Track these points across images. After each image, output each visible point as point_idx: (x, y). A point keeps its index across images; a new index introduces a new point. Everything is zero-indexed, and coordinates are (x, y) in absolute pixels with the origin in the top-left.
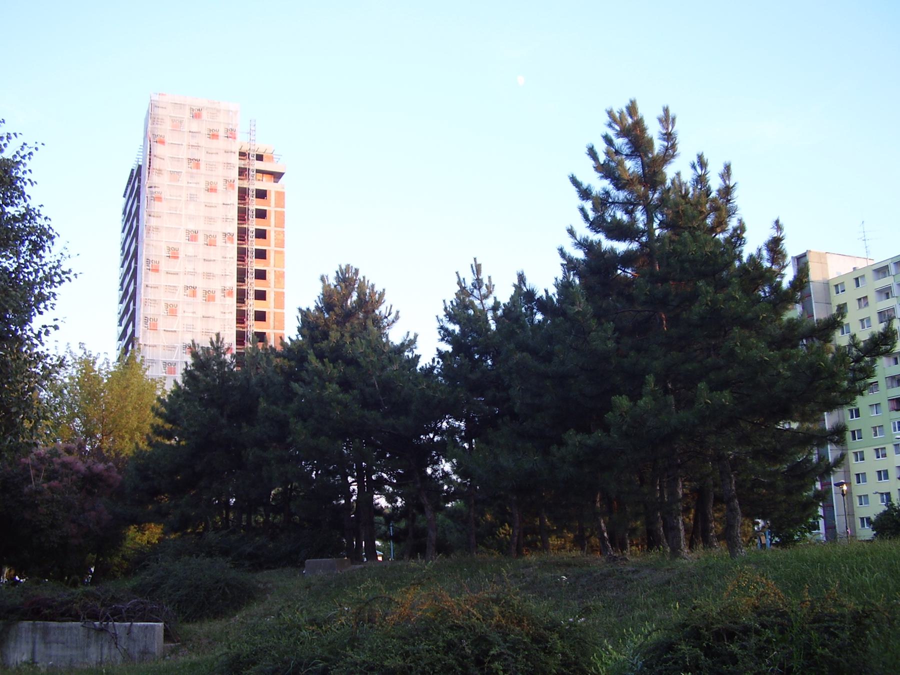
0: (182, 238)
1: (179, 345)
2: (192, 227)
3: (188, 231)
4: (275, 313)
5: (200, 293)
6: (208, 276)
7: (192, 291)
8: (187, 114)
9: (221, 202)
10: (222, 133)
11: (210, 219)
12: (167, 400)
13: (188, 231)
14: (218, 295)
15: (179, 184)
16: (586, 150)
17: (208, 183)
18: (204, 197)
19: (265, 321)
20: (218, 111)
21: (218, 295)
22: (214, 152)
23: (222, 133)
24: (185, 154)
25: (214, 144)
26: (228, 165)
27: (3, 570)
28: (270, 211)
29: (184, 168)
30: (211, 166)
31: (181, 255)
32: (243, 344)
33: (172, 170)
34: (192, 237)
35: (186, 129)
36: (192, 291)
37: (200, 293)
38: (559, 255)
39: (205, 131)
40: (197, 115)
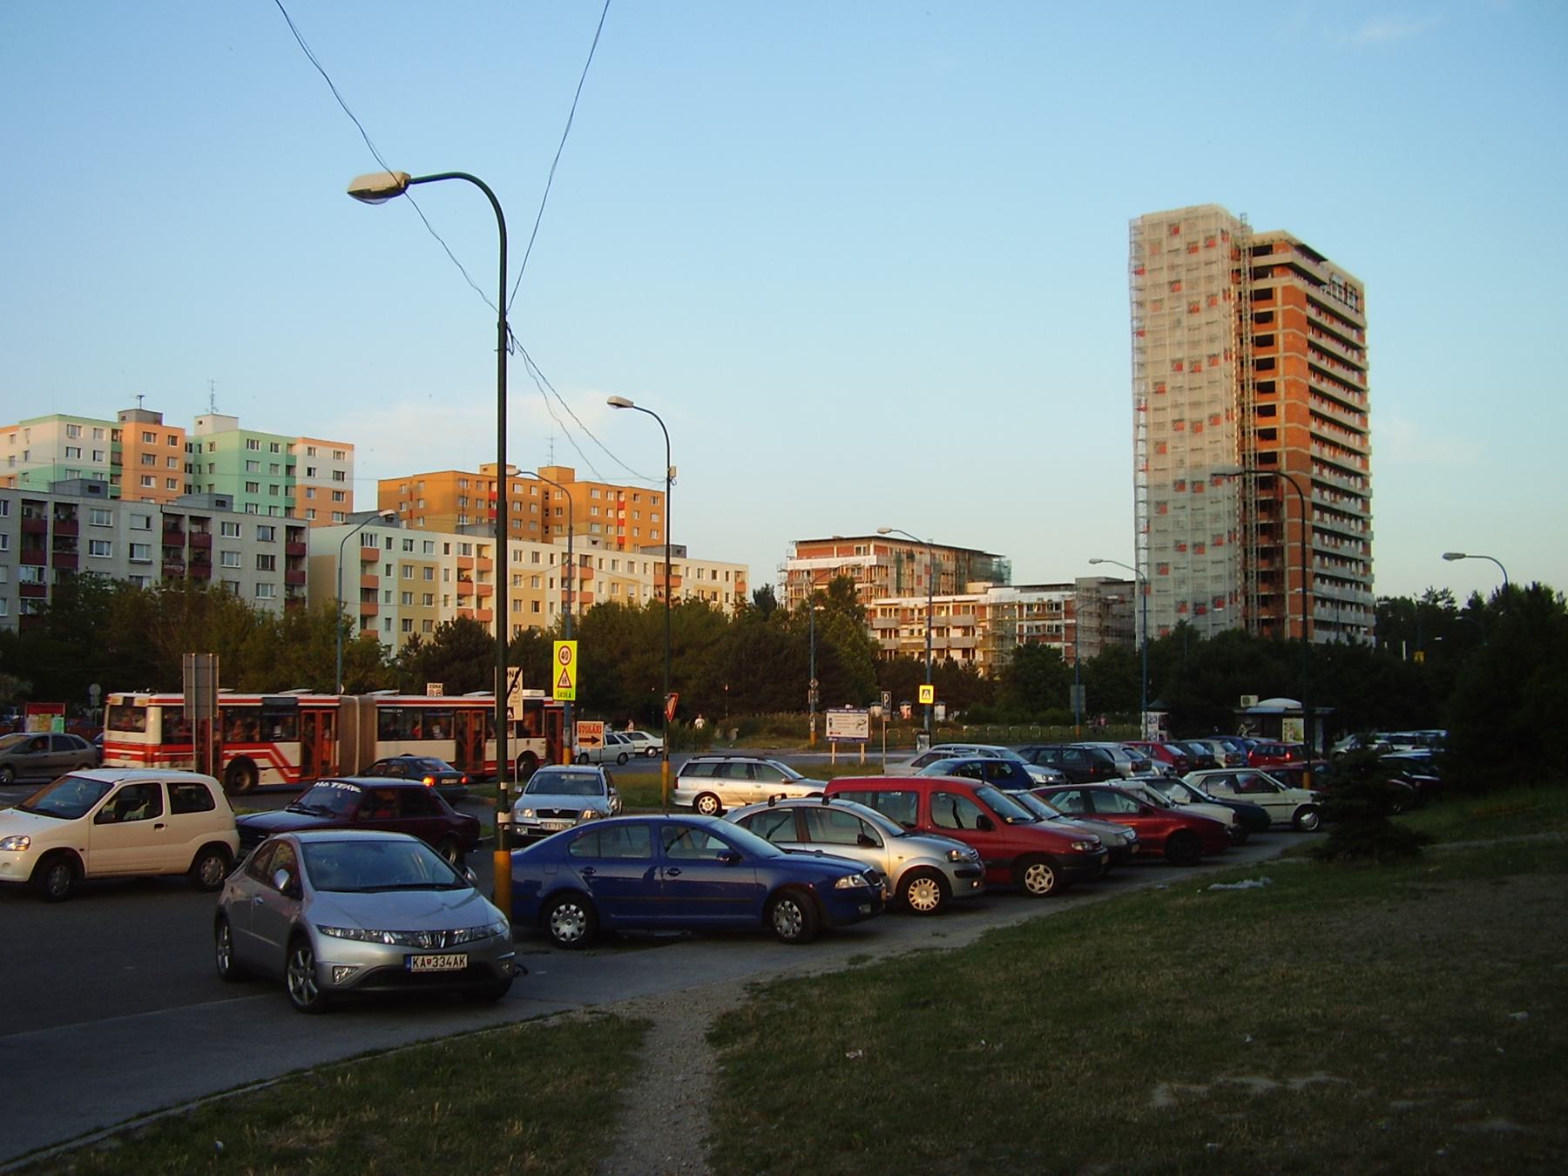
0: (1167, 369)
1: (1170, 482)
2: (1179, 355)
3: (1173, 362)
4: (1286, 429)
5: (1187, 425)
6: (1195, 405)
7: (1181, 548)
8: (1165, 230)
9: (1204, 322)
10: (1201, 244)
11: (1194, 344)
12: (730, 621)
13: (1173, 362)
14: (1206, 423)
15: (1163, 311)
16: (1446, 561)
17: (1190, 304)
18: (1188, 320)
19: (173, 813)
20: (1197, 218)
21: (1206, 423)
22: (1195, 266)
23: (1201, 244)
24: (1165, 277)
25: (1194, 258)
26: (1210, 279)
27: (341, 976)
28: (1277, 312)
29: (1165, 292)
30: (1193, 285)
31: (1168, 389)
32: (365, 628)
33: (1154, 298)
34: (1178, 366)
35: (1165, 250)
36: (1181, 548)
37: (1187, 425)
38: (368, 188)
39: (1183, 247)
40: (1175, 230)
